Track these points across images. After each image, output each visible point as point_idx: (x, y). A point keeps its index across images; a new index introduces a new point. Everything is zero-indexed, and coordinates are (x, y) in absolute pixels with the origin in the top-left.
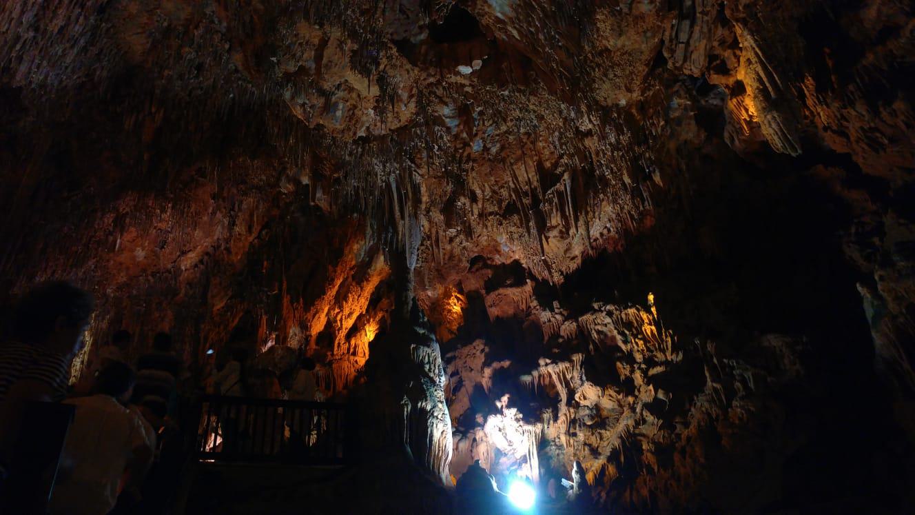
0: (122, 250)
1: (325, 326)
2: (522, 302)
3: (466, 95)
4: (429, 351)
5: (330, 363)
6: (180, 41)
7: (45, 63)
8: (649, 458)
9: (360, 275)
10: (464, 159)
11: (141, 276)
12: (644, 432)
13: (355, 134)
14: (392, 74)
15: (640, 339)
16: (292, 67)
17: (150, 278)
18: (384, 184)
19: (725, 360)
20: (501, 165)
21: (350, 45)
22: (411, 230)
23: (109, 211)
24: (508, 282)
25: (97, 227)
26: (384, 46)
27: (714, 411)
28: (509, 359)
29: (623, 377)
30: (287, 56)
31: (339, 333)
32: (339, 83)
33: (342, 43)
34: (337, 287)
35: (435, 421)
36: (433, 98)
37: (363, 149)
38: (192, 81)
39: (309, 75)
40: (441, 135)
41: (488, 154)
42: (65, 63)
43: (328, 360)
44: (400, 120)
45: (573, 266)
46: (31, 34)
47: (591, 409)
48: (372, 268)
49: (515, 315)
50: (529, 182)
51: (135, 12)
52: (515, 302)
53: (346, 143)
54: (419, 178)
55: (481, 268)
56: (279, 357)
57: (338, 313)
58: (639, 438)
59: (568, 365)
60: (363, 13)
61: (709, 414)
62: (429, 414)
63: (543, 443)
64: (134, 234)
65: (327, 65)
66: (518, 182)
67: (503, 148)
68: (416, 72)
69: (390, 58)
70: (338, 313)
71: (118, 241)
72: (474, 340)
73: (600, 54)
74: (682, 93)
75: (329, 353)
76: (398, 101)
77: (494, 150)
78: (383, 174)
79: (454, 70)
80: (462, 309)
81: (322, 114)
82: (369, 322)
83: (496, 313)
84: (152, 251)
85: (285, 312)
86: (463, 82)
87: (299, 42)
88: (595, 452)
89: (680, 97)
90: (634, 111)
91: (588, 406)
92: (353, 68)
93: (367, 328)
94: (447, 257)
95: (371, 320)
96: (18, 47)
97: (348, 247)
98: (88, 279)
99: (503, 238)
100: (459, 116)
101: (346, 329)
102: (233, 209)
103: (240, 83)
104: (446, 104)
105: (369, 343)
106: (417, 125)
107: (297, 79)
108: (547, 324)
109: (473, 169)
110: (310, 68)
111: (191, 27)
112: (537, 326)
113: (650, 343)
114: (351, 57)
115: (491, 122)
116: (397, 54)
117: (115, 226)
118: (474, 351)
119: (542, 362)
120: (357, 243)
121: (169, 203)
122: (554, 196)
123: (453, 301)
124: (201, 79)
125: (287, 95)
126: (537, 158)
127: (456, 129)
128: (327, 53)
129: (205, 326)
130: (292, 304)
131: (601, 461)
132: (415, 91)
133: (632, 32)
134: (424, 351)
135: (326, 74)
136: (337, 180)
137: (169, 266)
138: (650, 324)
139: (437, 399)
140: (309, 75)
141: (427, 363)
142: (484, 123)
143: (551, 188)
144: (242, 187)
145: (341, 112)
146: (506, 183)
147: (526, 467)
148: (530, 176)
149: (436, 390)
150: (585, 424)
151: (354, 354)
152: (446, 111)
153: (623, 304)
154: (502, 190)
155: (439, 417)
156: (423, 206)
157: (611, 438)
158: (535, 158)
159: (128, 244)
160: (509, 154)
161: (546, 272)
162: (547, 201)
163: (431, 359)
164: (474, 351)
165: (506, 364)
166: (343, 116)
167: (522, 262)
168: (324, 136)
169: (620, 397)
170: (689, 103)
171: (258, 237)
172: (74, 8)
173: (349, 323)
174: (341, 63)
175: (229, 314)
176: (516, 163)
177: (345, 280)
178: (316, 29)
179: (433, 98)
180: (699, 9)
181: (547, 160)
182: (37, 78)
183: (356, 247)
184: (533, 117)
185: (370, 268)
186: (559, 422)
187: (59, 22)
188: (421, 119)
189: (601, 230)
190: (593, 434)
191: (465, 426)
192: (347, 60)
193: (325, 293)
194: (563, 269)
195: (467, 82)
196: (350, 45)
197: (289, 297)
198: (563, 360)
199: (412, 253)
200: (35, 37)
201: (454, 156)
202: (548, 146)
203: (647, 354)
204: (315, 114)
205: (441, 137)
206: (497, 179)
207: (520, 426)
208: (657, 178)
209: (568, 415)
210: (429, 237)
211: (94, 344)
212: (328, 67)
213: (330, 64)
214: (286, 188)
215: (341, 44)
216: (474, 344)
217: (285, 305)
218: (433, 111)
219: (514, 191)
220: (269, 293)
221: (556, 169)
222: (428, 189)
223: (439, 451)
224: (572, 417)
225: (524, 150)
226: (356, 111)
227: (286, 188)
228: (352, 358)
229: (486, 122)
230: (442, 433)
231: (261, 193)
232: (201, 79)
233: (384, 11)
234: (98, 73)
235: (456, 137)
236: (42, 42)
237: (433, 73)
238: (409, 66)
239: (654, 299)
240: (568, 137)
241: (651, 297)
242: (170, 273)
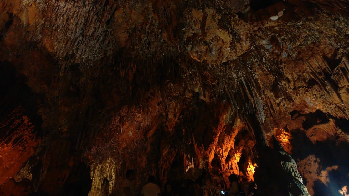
1: (214, 157)
2: (331, 132)
5: (221, 175)
6: (140, 33)
7: (87, 50)
9: (229, 130)
11: (131, 143)
13: (221, 61)
14: (237, 29)
17: (135, 144)
18: (239, 83)
21: (218, 17)
23: (117, 116)
24: (319, 121)
25: (113, 123)
31: (222, 159)
32: (212, 38)
37: (226, 68)
38: (147, 50)
39: (199, 36)
40: (265, 53)
41: (291, 58)
42: (95, 49)
44: (243, 51)
46: (81, 38)
48: (235, 126)
51: (121, 22)
52: (326, 132)
53: (218, 67)
54: (257, 76)
56: (194, 173)
57: (220, 150)
64: (128, 125)
65: (207, 29)
66: (313, 68)
67: (299, 53)
68: (248, 26)
69: (235, 21)
70: (220, 150)
71: (122, 129)
72: (308, 155)
75: (219, 170)
76: (241, 41)
77: (294, 55)
78: (237, 78)
79: (269, 20)
80: (289, 140)
81: (206, 55)
82: (236, 152)
83: (316, 139)
84: (135, 132)
85: (196, 151)
87: (193, 20)
92: (220, 28)
93: (235, 155)
95: (237, 151)
96: (76, 44)
97: (221, 118)
98: (111, 148)
102: (166, 108)
103: (167, 47)
104: (263, 39)
105: (238, 163)
106: (252, 51)
110: (199, 33)
111: (144, 26)
115: (289, 42)
116: (238, 19)
117: (120, 122)
118: (310, 162)
120: (225, 115)
121: (141, 109)
122: (339, 71)
124: (150, 49)
125: (189, 49)
127: (271, 50)
129: (161, 163)
132: (249, 35)
135: (208, 33)
136: (214, 86)
140: (199, 36)
142: (286, 44)
143: (336, 67)
145: (214, 52)
146: (305, 70)
148: (320, 64)
151: (232, 169)
152: (264, 42)
154: (304, 74)
159: (125, 130)
160: (304, 55)
162: (335, 74)
165: (336, 167)
166: (215, 54)
168: (208, 65)
171: (179, 119)
172: (97, 23)
173: (226, 154)
174: (214, 26)
175: (170, 155)
177: (221, 133)
178: (200, 12)
181: (328, 54)
183: (225, 117)
185: (234, 126)
187: (92, 30)
188: (253, 48)
193: (213, 141)
196: (218, 17)
197: (196, 144)
199: (261, 114)
200: (82, 39)
201: (274, 62)
202: (327, 46)
205: (265, 54)
206: (300, 69)
211: (116, 175)
213: (209, 28)
214: (188, 95)
216: (308, 158)
217: (196, 149)
218: (258, 43)
220: (187, 144)
221: (336, 57)
222: (262, 81)
225: (313, 51)
226: (222, 50)
228: (231, 171)
229: (287, 43)
231: (178, 99)
232: (150, 49)
234: (109, 52)
235: (272, 53)
236: (86, 41)
237: (256, 25)
238: (244, 23)
240: (340, 39)
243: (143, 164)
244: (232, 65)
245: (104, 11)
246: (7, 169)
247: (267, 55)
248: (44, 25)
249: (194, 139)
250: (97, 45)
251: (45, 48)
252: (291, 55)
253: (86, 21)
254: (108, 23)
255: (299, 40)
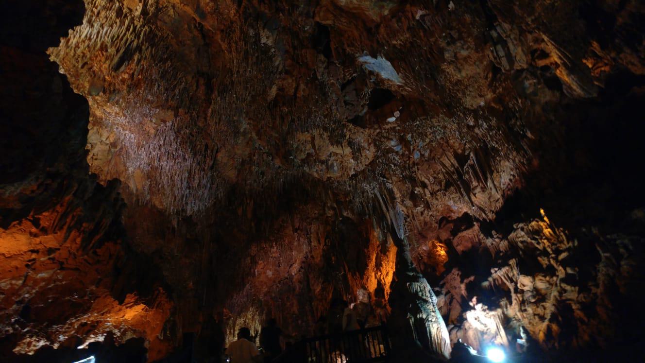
0: (260, 274)
3: (399, 132)
4: (419, 284)
7: (197, 201)
8: (579, 313)
9: (384, 251)
10: (411, 166)
12: (569, 297)
13: (348, 175)
14: (354, 138)
15: (544, 239)
16: (303, 156)
17: (278, 285)
19: (608, 236)
20: (433, 161)
21: (325, 135)
22: (396, 216)
24: (463, 228)
26: (344, 125)
27: (611, 272)
28: (473, 275)
29: (545, 266)
30: (298, 152)
33: (321, 135)
34: (374, 260)
35: (430, 323)
36: (383, 140)
37: (356, 181)
41: (424, 158)
43: (383, 304)
45: (499, 205)
46: (188, 191)
47: (532, 292)
48: (389, 243)
49: (473, 246)
50: (453, 165)
54: (391, 185)
55: (446, 224)
57: (381, 275)
58: (568, 302)
59: (507, 268)
60: (325, 117)
61: (608, 275)
62: (425, 320)
63: (506, 322)
67: (431, 151)
69: (350, 130)
73: (456, 84)
74: (528, 76)
75: (383, 300)
76: (363, 150)
77: (427, 154)
79: (386, 122)
80: (446, 252)
83: (461, 249)
85: (350, 282)
86: (394, 126)
88: (542, 318)
89: (528, 79)
90: (493, 105)
91: (529, 290)
94: (423, 224)
96: (184, 199)
99: (451, 203)
100: (401, 143)
101: (389, 283)
102: (307, 234)
104: (392, 139)
106: (378, 157)
107: (309, 160)
108: (492, 246)
109: (418, 169)
112: (486, 249)
113: (555, 240)
114: (329, 139)
119: (492, 271)
123: (439, 248)
126: (453, 150)
127: (402, 151)
128: (316, 143)
130: (353, 277)
131: (546, 322)
133: (466, 67)
134: (416, 286)
135: (320, 153)
136: (350, 201)
137: (286, 275)
138: (547, 228)
139: (429, 311)
141: (420, 292)
142: (415, 142)
143: (465, 165)
144: (308, 220)
147: (498, 338)
149: (428, 306)
150: (530, 302)
152: (393, 143)
153: (528, 221)
154: (439, 175)
155: (433, 320)
156: (399, 200)
157: (549, 307)
158: (451, 150)
161: (483, 215)
163: (422, 289)
164: (454, 276)
165: (472, 278)
166: (338, 169)
167: (469, 212)
169: (548, 278)
170: (535, 81)
171: (325, 245)
175: (325, 292)
176: (441, 157)
177: (377, 254)
179: (383, 140)
180: (504, 36)
181: (458, 149)
182: (196, 209)
184: (439, 129)
186: (513, 304)
187: (197, 181)
189: (509, 177)
190: (538, 307)
191: (455, 322)
192: (327, 142)
193: (368, 266)
194: (493, 209)
195: (396, 125)
197: (350, 273)
198: (504, 266)
200: (190, 191)
201: (405, 167)
202: (456, 140)
203: (554, 247)
204: (324, 173)
207: (487, 313)
208: (529, 135)
209: (518, 299)
210: (408, 216)
212: (319, 149)
215: (321, 135)
216: (453, 272)
217: (350, 279)
219: (446, 174)
221: (465, 153)
222: (398, 189)
223: (438, 340)
224: (521, 299)
227: (329, 213)
229: (417, 141)
230: (437, 329)
233: (337, 109)
235: (403, 155)
238: (362, 130)
239: (544, 212)
241: (542, 211)
242: (287, 279)
243: (295, 309)
244: (360, 177)
245: (205, 157)
246: (154, 328)
247: (397, 159)
248: (150, 185)
249: (346, 267)
250: (207, 191)
251: (155, 206)
252: (424, 155)
253: (190, 173)
254: (212, 168)
255: (427, 137)
